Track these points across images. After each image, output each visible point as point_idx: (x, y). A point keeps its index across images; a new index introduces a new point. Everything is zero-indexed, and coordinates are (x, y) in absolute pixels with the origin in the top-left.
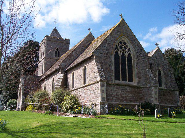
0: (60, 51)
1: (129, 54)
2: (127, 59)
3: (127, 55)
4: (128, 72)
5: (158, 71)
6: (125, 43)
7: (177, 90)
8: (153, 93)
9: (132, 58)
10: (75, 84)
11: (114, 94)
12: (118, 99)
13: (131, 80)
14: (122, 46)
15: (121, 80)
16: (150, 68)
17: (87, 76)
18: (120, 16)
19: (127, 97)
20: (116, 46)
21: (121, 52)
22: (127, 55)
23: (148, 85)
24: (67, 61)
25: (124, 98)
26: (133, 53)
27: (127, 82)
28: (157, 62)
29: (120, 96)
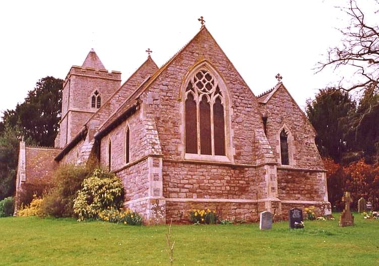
1: (218, 99)
3: (212, 100)
5: (280, 132)
6: (209, 77)
7: (320, 171)
9: (225, 107)
13: (221, 151)
14: (202, 83)
17: (131, 146)
18: (199, 20)
19: (212, 188)
20: (190, 83)
22: (212, 100)
24: (101, 117)
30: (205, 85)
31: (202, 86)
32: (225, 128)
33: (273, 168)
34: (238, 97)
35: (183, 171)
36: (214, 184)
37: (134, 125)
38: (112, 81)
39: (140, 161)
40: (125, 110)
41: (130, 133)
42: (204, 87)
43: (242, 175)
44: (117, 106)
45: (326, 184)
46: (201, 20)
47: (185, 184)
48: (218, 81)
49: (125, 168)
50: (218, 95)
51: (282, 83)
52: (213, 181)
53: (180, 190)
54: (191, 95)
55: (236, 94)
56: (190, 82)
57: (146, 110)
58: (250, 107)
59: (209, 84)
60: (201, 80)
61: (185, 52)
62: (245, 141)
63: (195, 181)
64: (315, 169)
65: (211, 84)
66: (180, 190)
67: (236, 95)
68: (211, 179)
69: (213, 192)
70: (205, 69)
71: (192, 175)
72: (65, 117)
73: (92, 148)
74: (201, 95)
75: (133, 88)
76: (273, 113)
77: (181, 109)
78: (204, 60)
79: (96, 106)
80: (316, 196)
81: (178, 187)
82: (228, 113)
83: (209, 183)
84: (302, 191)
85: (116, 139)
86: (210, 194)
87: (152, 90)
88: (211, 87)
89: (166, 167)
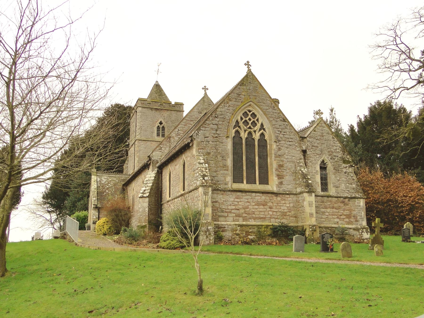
0: (165, 126)
1: (262, 135)
2: (256, 143)
3: (257, 136)
4: (247, 168)
5: (319, 163)
6: (254, 115)
7: (359, 198)
8: (306, 204)
9: (268, 141)
10: (171, 190)
11: (229, 207)
12: (238, 216)
13: (264, 180)
14: (248, 121)
15: (245, 182)
16: (302, 157)
17: (186, 177)
18: (245, 64)
19: (256, 213)
20: (237, 121)
21: (245, 131)
22: (257, 136)
23: (298, 189)
24: (163, 149)
25: (249, 214)
26: (270, 132)
27: (258, 187)
28: (317, 147)
29: (242, 211)
30: (250, 122)
31: (248, 123)
32: (269, 160)
33: (311, 195)
34: (281, 132)
35: (231, 198)
36: (258, 209)
37: (189, 159)
38: (175, 112)
39: (194, 190)
40: (174, 151)
41: (186, 166)
42: (250, 124)
43: (284, 202)
44: (177, 139)
45: (365, 210)
46: (248, 64)
47: (232, 209)
48: (262, 119)
49: (182, 195)
50: (262, 131)
51: (322, 118)
52: (256, 207)
53: (228, 215)
54: (237, 132)
55: (279, 130)
56: (237, 120)
57: (198, 147)
58: (291, 141)
59: (254, 121)
60: (247, 119)
61: (232, 94)
62: (286, 171)
63: (241, 207)
64: (353, 196)
65: (256, 122)
66: (228, 215)
67: (279, 131)
68: (255, 205)
69: (257, 216)
70: (250, 109)
71: (238, 202)
72: (133, 145)
73: (155, 177)
74: (247, 132)
75: (192, 123)
76: (313, 146)
77: (229, 145)
78: (249, 101)
79: (161, 135)
80: (354, 220)
81: (226, 212)
82: (271, 147)
83: (253, 208)
84: (341, 215)
85: (175, 169)
86: (254, 218)
87: (203, 129)
88: (256, 124)
89: (215, 195)
